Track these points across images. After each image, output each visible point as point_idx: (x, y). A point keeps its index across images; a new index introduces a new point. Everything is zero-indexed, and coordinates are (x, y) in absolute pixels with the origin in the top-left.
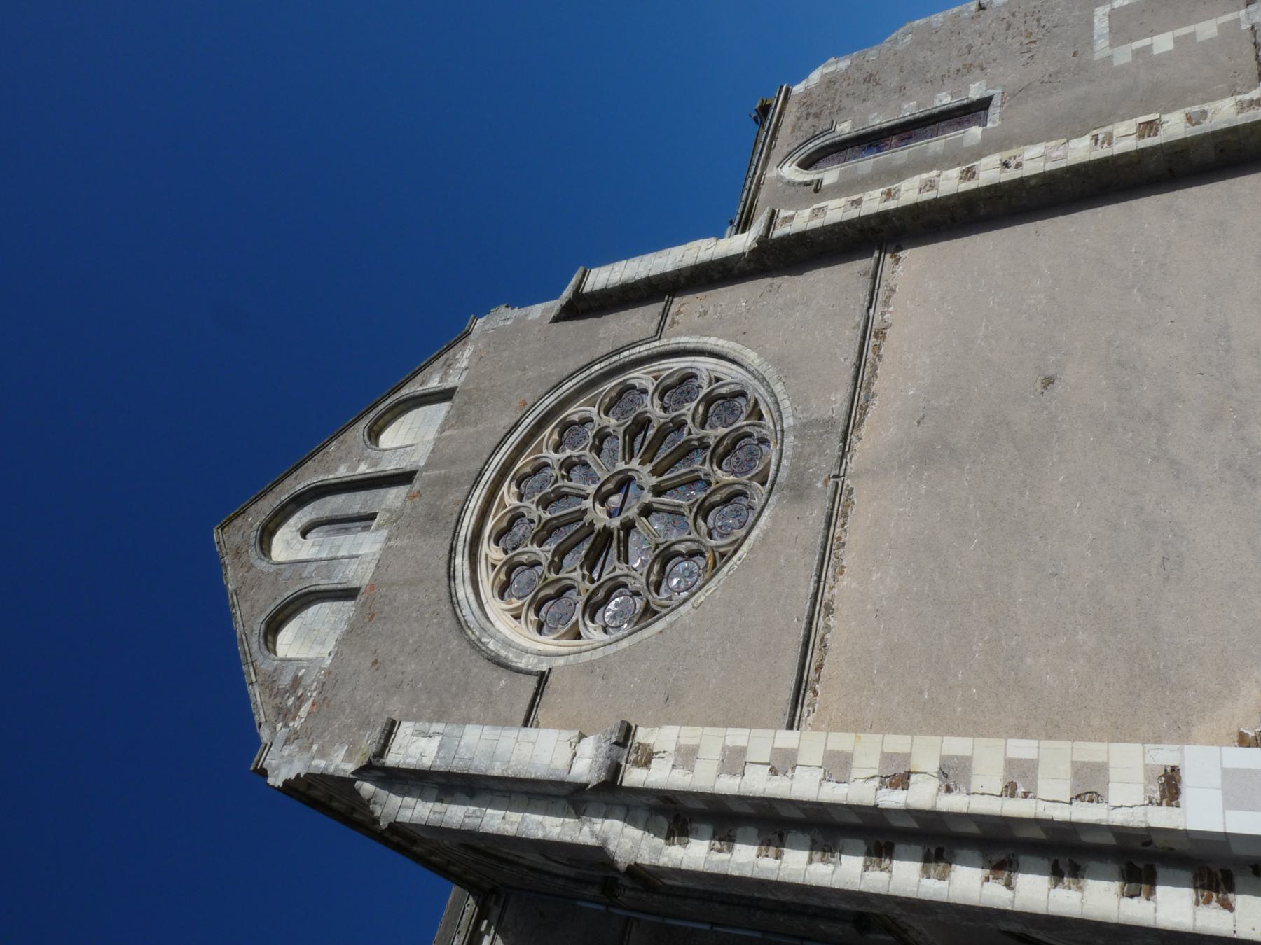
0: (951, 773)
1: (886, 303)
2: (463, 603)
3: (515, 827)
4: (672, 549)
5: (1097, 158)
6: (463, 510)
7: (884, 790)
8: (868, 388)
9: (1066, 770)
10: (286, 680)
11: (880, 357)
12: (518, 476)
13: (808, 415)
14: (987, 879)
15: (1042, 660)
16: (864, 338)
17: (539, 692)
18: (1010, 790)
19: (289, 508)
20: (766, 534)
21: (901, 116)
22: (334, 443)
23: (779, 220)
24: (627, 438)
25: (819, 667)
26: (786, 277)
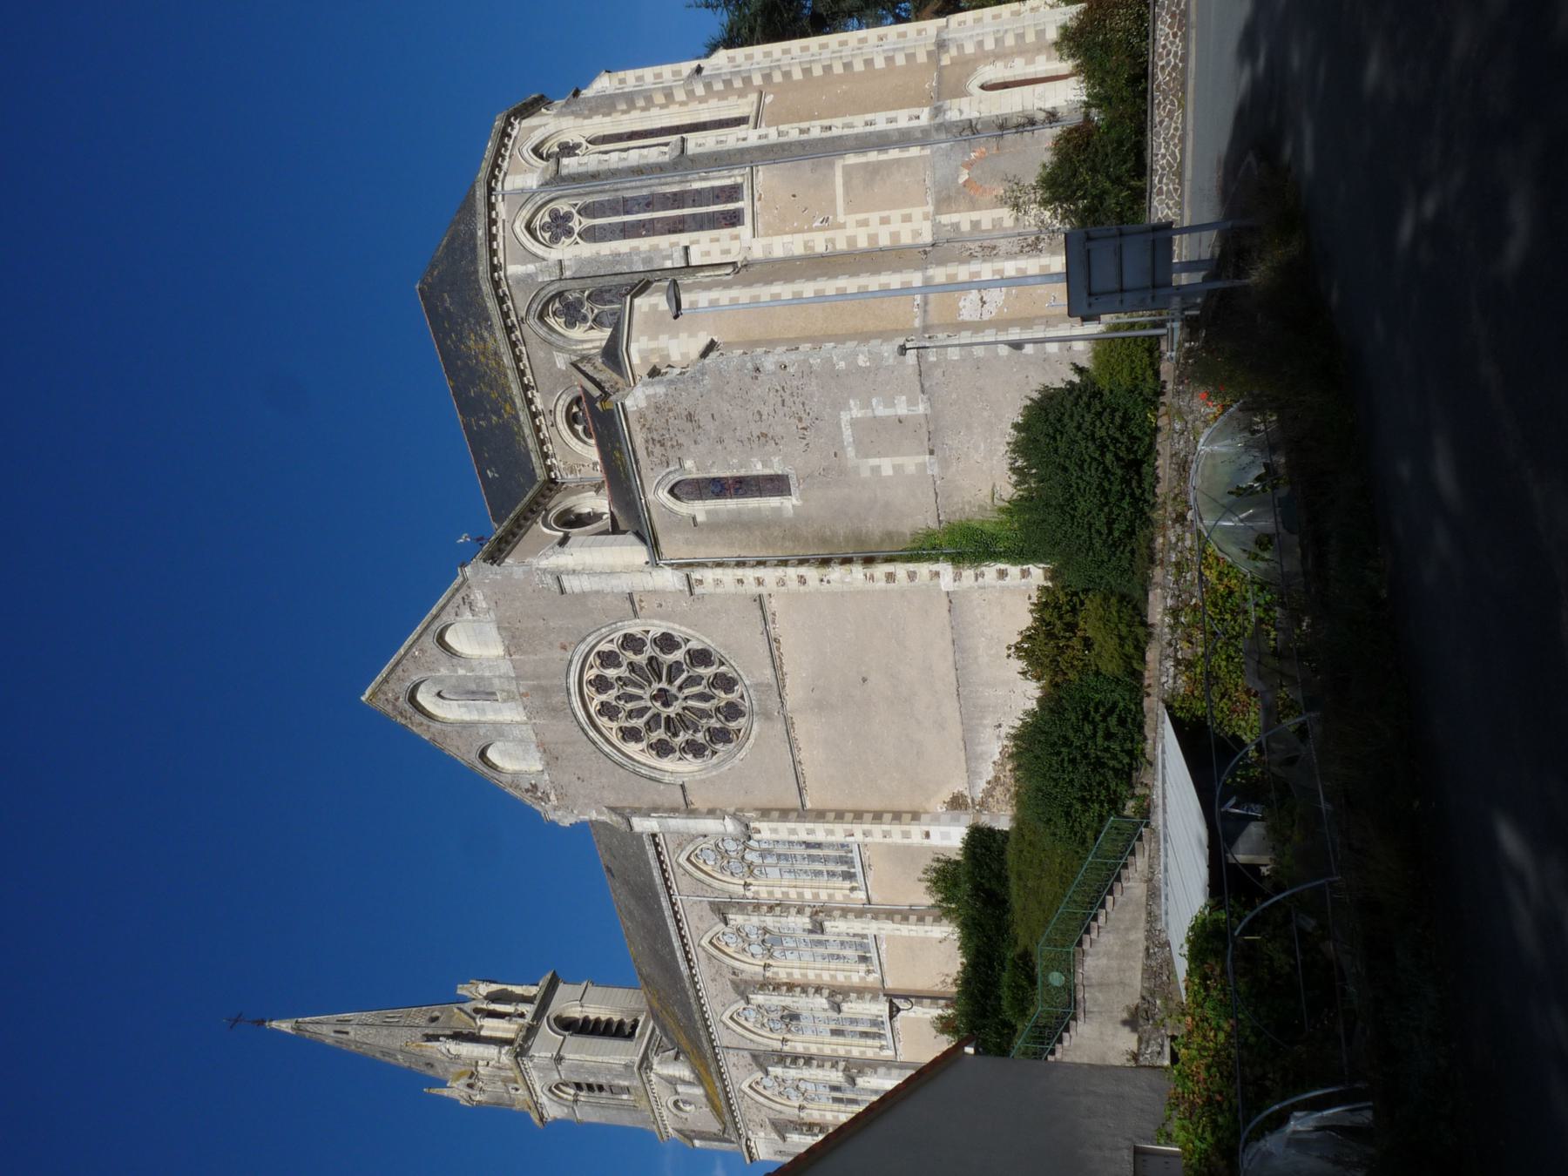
1: (774, 622)
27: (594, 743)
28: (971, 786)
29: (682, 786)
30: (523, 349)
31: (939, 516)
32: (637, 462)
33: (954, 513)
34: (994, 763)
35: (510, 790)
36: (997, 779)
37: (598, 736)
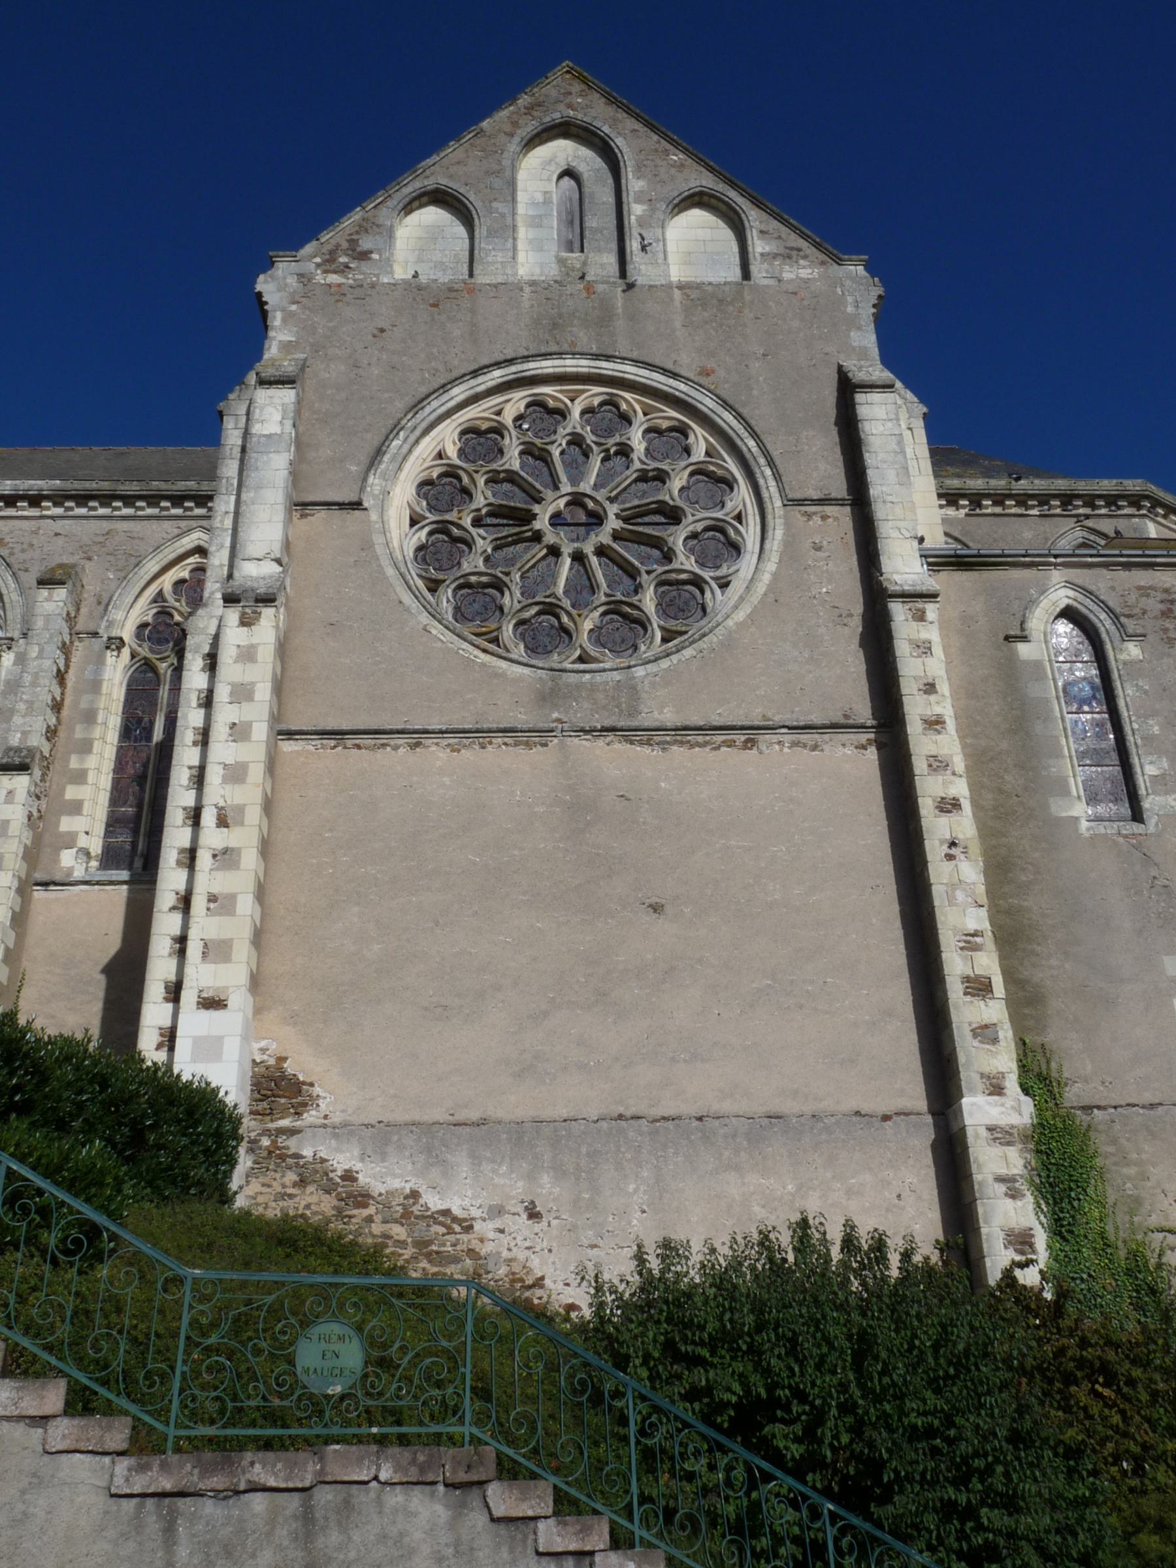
0: (227, 857)
1: (795, 744)
2: (445, 397)
3: (218, 525)
4: (505, 589)
5: (941, 937)
6: (560, 354)
7: (215, 810)
8: (675, 742)
9: (225, 935)
10: (365, 243)
11: (718, 748)
12: (615, 399)
13: (647, 688)
14: (177, 894)
15: (356, 920)
16: (742, 728)
17: (342, 506)
18: (212, 898)
19: (597, 140)
20: (503, 675)
21: (1133, 718)
22: (681, 156)
23: (920, 605)
24: (653, 506)
25: (358, 747)
26: (860, 629)
27: (475, 373)
28: (341, 1131)
29: (357, 505)
30: (1035, 512)
31: (1099, 1108)
32: (1127, 566)
33: (1114, 1141)
34: (415, 1195)
35: (357, 215)
36: (362, 1198)
37: (491, 384)
